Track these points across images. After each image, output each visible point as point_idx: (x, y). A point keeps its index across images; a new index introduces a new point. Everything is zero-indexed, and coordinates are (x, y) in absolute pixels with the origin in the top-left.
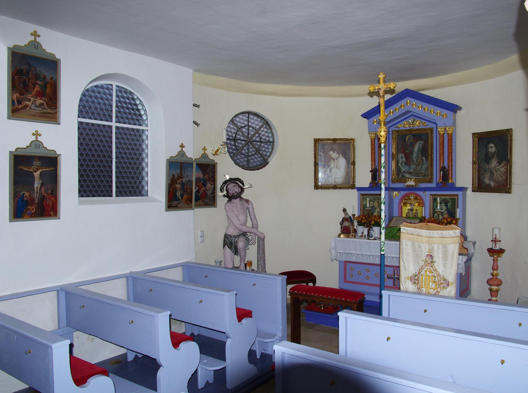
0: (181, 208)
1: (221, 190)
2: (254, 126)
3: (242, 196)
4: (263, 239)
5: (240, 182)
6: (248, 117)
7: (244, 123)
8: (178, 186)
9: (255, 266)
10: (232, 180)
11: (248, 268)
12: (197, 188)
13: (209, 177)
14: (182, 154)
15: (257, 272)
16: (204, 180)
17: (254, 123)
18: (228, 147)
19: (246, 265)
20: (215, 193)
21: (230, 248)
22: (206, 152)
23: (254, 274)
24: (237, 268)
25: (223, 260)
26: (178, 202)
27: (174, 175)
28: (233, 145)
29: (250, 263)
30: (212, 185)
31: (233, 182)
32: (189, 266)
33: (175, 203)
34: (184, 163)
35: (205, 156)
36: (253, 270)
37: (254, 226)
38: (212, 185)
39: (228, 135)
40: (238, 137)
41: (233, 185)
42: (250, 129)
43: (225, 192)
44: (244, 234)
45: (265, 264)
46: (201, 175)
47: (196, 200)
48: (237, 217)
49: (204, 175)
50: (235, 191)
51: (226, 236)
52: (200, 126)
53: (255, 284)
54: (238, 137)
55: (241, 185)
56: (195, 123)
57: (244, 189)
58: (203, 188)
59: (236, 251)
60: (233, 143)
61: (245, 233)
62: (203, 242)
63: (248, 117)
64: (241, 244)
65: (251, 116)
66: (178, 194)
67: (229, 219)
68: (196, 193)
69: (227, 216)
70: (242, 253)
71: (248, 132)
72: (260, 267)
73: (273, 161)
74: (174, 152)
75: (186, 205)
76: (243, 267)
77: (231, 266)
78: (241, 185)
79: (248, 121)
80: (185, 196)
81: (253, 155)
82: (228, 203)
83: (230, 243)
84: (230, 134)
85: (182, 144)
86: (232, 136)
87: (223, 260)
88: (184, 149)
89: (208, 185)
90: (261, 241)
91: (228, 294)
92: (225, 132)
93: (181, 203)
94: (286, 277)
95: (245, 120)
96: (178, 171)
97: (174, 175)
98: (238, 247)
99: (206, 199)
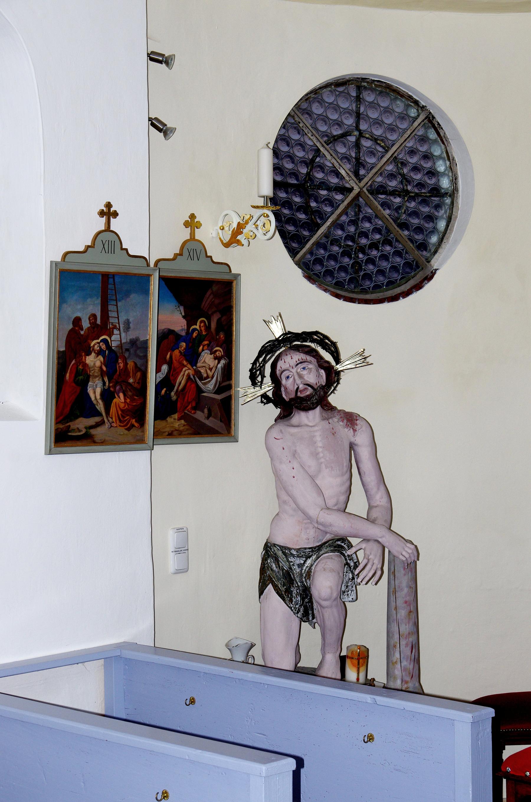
0: (103, 443)
1: (253, 378)
2: (378, 132)
3: (332, 399)
4: (412, 567)
5: (325, 347)
6: (358, 99)
7: (339, 124)
8: (93, 361)
9: (377, 669)
10: (291, 341)
11: (351, 674)
12: (165, 368)
13: (208, 328)
14: (107, 239)
15: (387, 689)
16: (188, 337)
17: (378, 123)
18: (277, 215)
19: (343, 660)
20: (229, 387)
21: (285, 595)
22: (199, 235)
23: (368, 698)
24: (311, 673)
25: (258, 642)
26: (92, 421)
27: (77, 321)
28: (299, 209)
29: (362, 657)
30: (219, 359)
31: (297, 349)
32: (128, 661)
33: (81, 424)
34: (113, 275)
35: (192, 248)
36: (370, 683)
37: (375, 514)
38: (219, 359)
39: (277, 169)
40: (319, 175)
41: (298, 356)
42: (366, 143)
43: (268, 387)
44: (338, 545)
45: (417, 661)
46: (177, 321)
47: (159, 415)
48: (312, 478)
49: (190, 319)
50: (308, 383)
51: (269, 550)
52: (174, 137)
53: (370, 738)
54: (319, 175)
55: (327, 356)
56: (156, 124)
57: (338, 373)
58: (187, 371)
59: (307, 610)
60: (297, 199)
61: (343, 539)
62: (182, 570)
63: (358, 99)
64: (325, 581)
65: (369, 97)
66: (95, 390)
67: (281, 485)
68: (158, 387)
69: (276, 474)
70: (328, 614)
71: (357, 159)
72: (398, 672)
73: (454, 265)
74: (80, 235)
75: (122, 430)
76: (331, 669)
77: (288, 664)
78: (327, 356)
79: (358, 116)
80: (120, 399)
81: (374, 246)
82: (281, 426)
83: (283, 575)
84: (289, 166)
85: (109, 205)
86: (295, 174)
87: (258, 642)
88: (115, 224)
89: (207, 359)
90: (404, 573)
91: (263, 768)
92: (267, 160)
93: (102, 423)
94: (490, 712)
95: (347, 111)
96: (94, 307)
97: (77, 321)
98: (315, 592)
99: (204, 415)
